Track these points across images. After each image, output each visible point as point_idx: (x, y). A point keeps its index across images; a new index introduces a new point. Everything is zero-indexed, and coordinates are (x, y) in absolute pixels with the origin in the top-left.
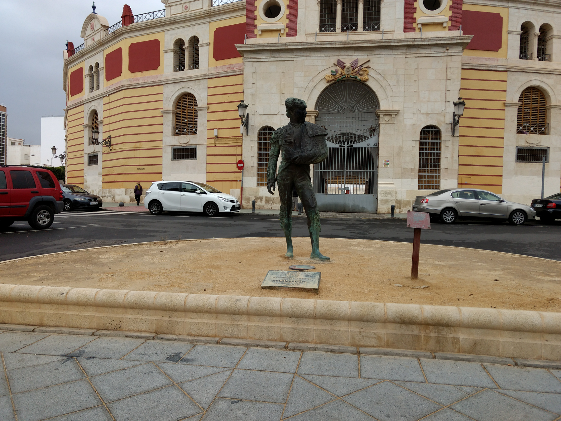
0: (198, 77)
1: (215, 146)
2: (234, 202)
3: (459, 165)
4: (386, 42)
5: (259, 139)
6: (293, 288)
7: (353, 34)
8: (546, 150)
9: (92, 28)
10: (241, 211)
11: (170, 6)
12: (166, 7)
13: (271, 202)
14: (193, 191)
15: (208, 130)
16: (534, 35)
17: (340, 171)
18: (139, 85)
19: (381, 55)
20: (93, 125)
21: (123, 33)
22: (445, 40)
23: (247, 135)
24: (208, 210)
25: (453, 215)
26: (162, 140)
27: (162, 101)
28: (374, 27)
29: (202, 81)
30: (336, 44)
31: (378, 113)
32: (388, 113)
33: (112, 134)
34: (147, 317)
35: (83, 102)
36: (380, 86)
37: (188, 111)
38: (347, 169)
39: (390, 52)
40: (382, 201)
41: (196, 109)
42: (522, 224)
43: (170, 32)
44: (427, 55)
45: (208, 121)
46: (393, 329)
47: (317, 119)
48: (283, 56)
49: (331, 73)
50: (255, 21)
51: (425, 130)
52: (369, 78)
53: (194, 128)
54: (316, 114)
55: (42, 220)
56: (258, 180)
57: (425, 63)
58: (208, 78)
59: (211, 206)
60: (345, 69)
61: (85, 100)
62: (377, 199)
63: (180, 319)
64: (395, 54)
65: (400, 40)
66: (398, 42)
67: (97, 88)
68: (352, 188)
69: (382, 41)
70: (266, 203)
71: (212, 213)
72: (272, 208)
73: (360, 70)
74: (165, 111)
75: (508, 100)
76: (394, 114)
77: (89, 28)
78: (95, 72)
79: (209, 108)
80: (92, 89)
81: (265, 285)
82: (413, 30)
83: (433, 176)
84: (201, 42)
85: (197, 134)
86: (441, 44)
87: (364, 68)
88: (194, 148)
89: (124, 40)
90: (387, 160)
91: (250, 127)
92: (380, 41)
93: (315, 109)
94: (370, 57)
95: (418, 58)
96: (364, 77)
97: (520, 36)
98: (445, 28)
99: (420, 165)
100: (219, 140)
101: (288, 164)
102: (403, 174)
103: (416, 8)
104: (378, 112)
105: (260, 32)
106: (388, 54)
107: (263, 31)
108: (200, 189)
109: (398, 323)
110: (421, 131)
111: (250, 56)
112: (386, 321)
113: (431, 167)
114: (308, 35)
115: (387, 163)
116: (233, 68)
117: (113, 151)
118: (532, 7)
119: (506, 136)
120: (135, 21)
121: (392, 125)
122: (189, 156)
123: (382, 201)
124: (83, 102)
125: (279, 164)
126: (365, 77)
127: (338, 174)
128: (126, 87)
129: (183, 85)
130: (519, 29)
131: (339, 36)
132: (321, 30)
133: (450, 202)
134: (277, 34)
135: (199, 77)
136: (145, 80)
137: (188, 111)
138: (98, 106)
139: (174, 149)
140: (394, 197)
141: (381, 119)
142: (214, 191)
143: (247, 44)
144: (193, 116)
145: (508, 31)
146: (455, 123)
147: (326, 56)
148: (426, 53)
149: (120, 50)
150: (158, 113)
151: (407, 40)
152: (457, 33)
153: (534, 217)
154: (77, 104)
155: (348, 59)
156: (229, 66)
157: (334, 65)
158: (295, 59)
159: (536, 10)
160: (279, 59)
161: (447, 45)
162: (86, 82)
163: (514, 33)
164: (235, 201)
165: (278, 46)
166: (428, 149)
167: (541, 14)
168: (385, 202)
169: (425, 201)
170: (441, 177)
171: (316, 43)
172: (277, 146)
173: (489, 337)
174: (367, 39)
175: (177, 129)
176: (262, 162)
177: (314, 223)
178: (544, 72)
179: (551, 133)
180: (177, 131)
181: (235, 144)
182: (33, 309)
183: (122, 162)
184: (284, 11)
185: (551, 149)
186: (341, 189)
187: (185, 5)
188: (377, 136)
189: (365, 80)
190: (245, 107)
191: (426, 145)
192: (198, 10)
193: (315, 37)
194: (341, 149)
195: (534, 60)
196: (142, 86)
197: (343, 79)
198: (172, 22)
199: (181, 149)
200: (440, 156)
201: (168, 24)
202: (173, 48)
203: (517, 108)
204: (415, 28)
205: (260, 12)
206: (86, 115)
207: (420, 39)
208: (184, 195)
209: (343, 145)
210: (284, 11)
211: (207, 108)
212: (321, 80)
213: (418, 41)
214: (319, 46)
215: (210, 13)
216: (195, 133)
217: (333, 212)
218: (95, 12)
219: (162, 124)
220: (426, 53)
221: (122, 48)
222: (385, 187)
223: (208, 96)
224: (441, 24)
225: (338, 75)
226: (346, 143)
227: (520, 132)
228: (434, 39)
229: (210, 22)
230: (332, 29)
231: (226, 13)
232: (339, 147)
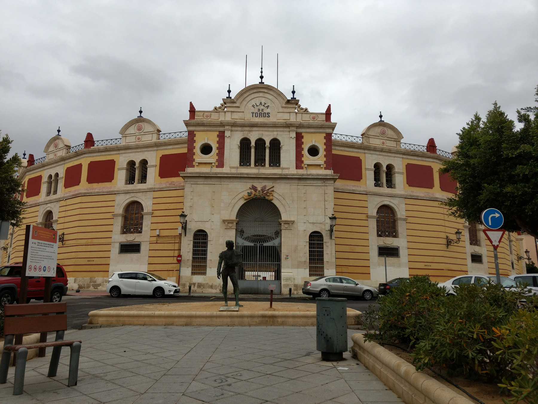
0: (145, 190)
1: (157, 243)
2: (176, 287)
3: (336, 258)
4: (284, 175)
5: (194, 239)
7: (263, 168)
8: (398, 249)
9: (56, 146)
10: (180, 294)
11: (126, 137)
12: (122, 137)
13: (202, 287)
14: (145, 278)
15: (151, 230)
18: (95, 193)
20: (46, 223)
21: (85, 153)
23: (185, 236)
24: (156, 293)
25: (327, 294)
26: (111, 238)
27: (114, 206)
28: (277, 165)
29: (148, 192)
30: (250, 175)
31: (280, 222)
32: (287, 223)
33: (66, 231)
34: (183, 320)
35: (39, 204)
36: (281, 204)
37: (135, 215)
38: (259, 262)
41: (142, 214)
42: (370, 300)
43: (124, 155)
44: (311, 185)
45: (151, 223)
46: (260, 319)
47: (237, 225)
48: (213, 181)
49: (248, 194)
50: (194, 156)
51: (312, 234)
52: (274, 198)
53: (140, 228)
54: (237, 222)
55: (55, 299)
56: (192, 270)
58: (154, 191)
59: (159, 290)
60: (257, 191)
61: (41, 202)
62: (281, 284)
63: (194, 320)
65: (293, 175)
66: (292, 176)
67: (54, 193)
68: (263, 274)
70: (198, 287)
71: (160, 295)
72: (202, 292)
73: (267, 193)
74: (116, 214)
75: (370, 214)
76: (291, 223)
77: (52, 145)
78: (53, 180)
79: (153, 213)
80: (49, 194)
81: (220, 310)
82: (302, 168)
84: (149, 164)
85: (142, 233)
88: (138, 244)
89: (85, 159)
91: (187, 230)
92: (280, 175)
93: (236, 218)
94: (274, 184)
95: (306, 187)
97: (373, 171)
98: (322, 168)
100: (160, 238)
102: (299, 266)
103: (303, 154)
105: (197, 164)
107: (199, 163)
108: (151, 277)
109: (262, 317)
110: (310, 235)
111: (189, 180)
112: (258, 317)
113: (317, 260)
114: (231, 168)
116: (174, 185)
117: (65, 246)
118: (380, 153)
119: (370, 238)
120: (95, 145)
122: (135, 250)
123: (284, 285)
124: (39, 204)
125: (222, 266)
126: (271, 197)
127: (250, 265)
128: (83, 194)
129: (132, 195)
130: (373, 167)
132: (240, 165)
133: (325, 285)
134: (210, 166)
135: (147, 190)
136: (100, 190)
137: (135, 215)
138: (55, 209)
139: (121, 245)
140: (293, 282)
141: (282, 226)
142: (161, 279)
143: (187, 172)
144: (139, 219)
146: (331, 231)
149: (80, 166)
150: (109, 216)
152: (330, 172)
153: (378, 295)
154: (32, 205)
155: (259, 185)
156: (171, 183)
158: (222, 183)
159: (383, 155)
160: (211, 183)
161: (324, 179)
162: (44, 188)
163: (369, 169)
164: (177, 286)
165: (210, 174)
166: (315, 247)
167: (387, 158)
168: (286, 286)
170: (325, 268)
172: (222, 259)
173: (287, 320)
174: (272, 173)
175: (125, 229)
176: (196, 256)
177: (237, 291)
178: (391, 196)
179: (399, 237)
180: (125, 230)
181: (173, 242)
182: (141, 319)
183: (74, 255)
184: (215, 151)
185: (400, 248)
187: (138, 137)
188: (280, 238)
190: (185, 216)
192: (148, 141)
193: (236, 169)
194: (255, 246)
195: (384, 187)
196: (97, 194)
198: (127, 148)
199: (127, 245)
200: (323, 253)
201: (123, 149)
202: (126, 167)
203: (376, 220)
204: (303, 167)
205: (197, 150)
206: (41, 214)
208: (138, 282)
209: (256, 244)
210: (215, 151)
211: (151, 213)
214: (239, 176)
215: (158, 144)
216: (141, 232)
218: (59, 134)
219: (113, 225)
221: (82, 164)
222: (286, 275)
223: (153, 204)
224: (320, 165)
225: (252, 196)
226: (258, 242)
227: (379, 236)
229: (157, 150)
230: (248, 164)
231: (170, 145)
232: (253, 245)
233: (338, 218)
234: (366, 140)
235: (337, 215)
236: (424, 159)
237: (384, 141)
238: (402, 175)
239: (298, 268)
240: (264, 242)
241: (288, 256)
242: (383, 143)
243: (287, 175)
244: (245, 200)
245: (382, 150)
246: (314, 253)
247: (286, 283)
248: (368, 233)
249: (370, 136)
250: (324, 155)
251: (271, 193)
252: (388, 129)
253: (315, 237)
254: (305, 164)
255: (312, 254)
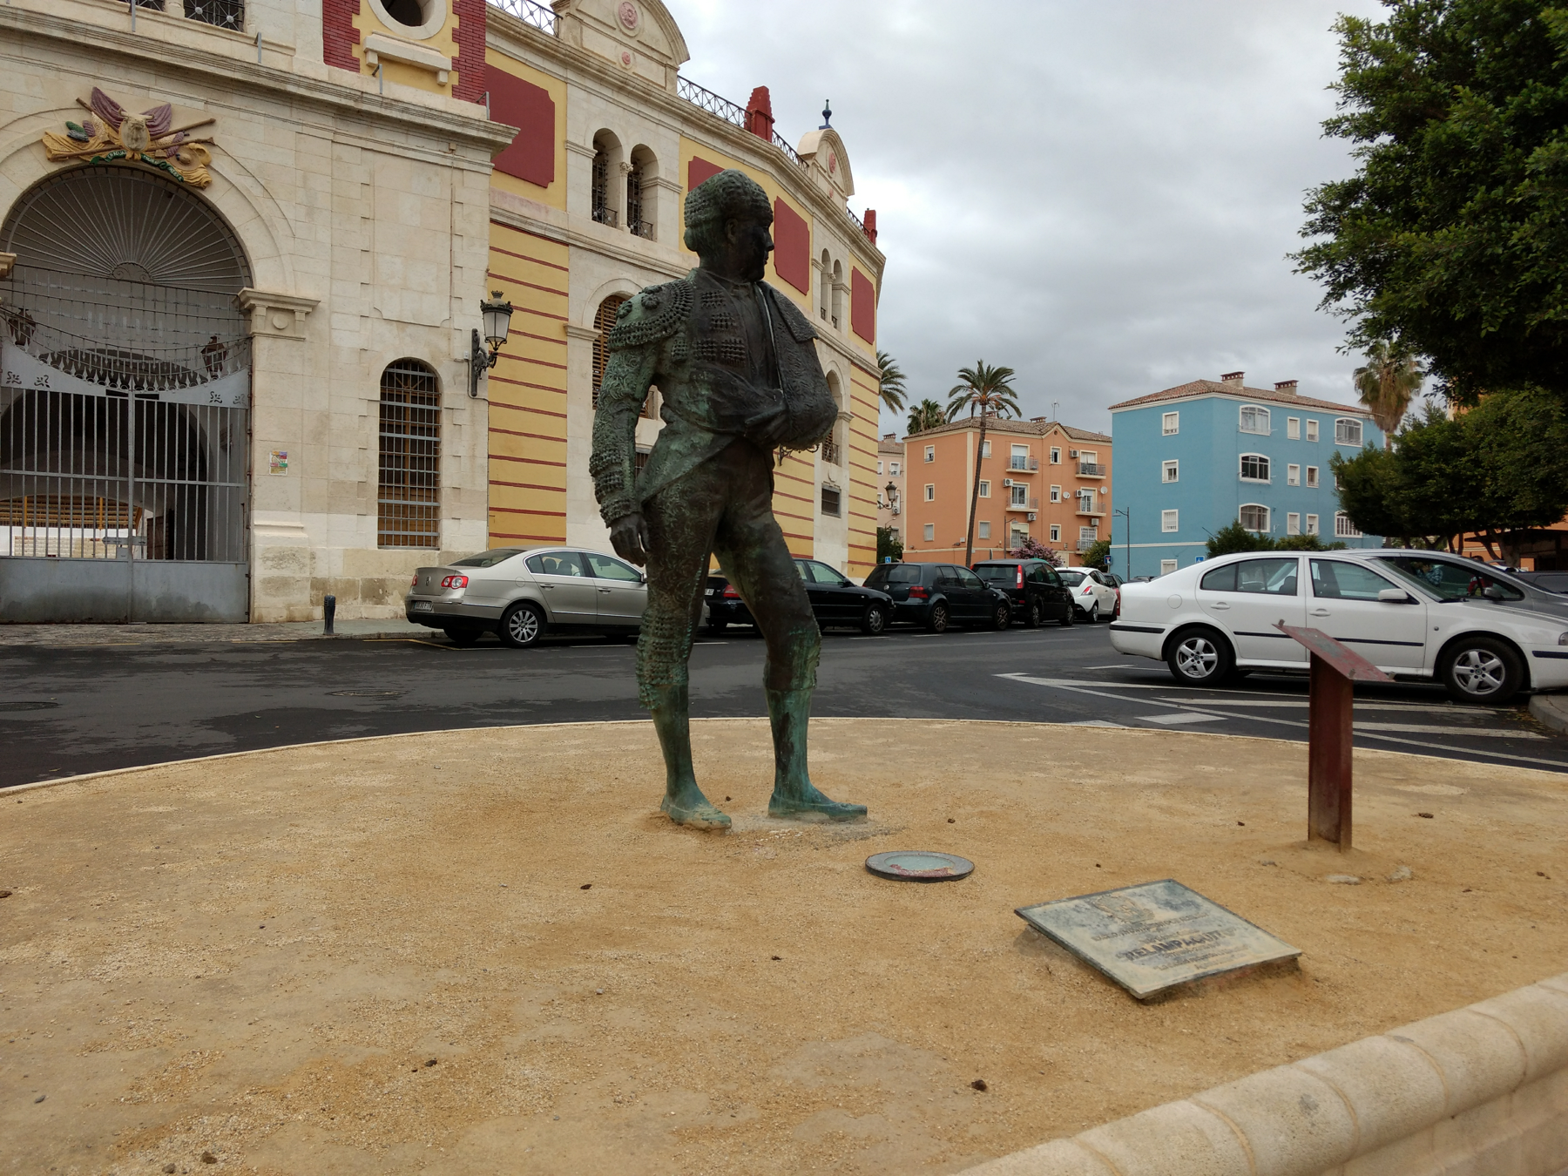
4: (272, 77)
6: (1238, 973)
7: (151, 17)
16: (619, 168)
17: (112, 478)
19: (253, 113)
22: (449, 123)
25: (533, 623)
30: (86, 32)
31: (248, 299)
32: (283, 305)
36: (253, 214)
38: (138, 474)
39: (284, 112)
40: (269, 583)
44: (396, 151)
57: (391, 172)
60: (124, 128)
62: (249, 576)
64: (298, 124)
66: (308, 87)
69: (257, 68)
75: (574, 321)
76: (301, 312)
82: (354, 65)
83: (421, 507)
86: (436, 128)
87: (197, 142)
90: (281, 450)
92: (248, 68)
94: (214, 112)
95: (370, 154)
96: (195, 171)
98: (442, 85)
99: (381, 473)
101: (726, 441)
102: (334, 499)
104: (248, 295)
106: (278, 118)
110: (385, 373)
113: (413, 481)
115: (280, 463)
118: (616, 96)
121: (295, 343)
123: (268, 582)
126: (197, 174)
130: (590, 145)
131: (94, 9)
140: (307, 569)
145: (567, 142)
147: (45, 67)
148: (394, 145)
151: (339, 88)
157: (79, 106)
161: (453, 138)
167: (635, 119)
169: (457, 582)
170: (444, 512)
171: (8, 10)
178: (643, 264)
186: (117, 541)
189: (200, 183)
191: (399, 417)
194: (113, 402)
197: (116, 162)
204: (358, 60)
207: (377, 98)
209: (119, 389)
212: (27, 147)
213: (371, 102)
217: (83, 622)
220: (394, 145)
222: (278, 538)
224: (433, 72)
225: (94, 145)
226: (132, 383)
228: (417, 109)
232: (104, 395)
233: (517, 308)
234: (569, 28)
235: (511, 295)
236: (740, 154)
237: (630, 52)
238: (676, 195)
239: (329, 511)
240: (172, 383)
241: (284, 457)
242: (626, 60)
243: (284, 77)
244: (55, 159)
245: (622, 87)
246: (398, 450)
247: (275, 573)
248: (566, 392)
249: (586, 20)
250: (454, 30)
251: (198, 149)
252: (642, 8)
253: (406, 384)
254: (368, 46)
255: (390, 457)
